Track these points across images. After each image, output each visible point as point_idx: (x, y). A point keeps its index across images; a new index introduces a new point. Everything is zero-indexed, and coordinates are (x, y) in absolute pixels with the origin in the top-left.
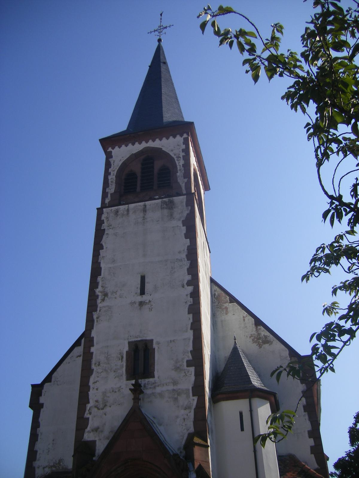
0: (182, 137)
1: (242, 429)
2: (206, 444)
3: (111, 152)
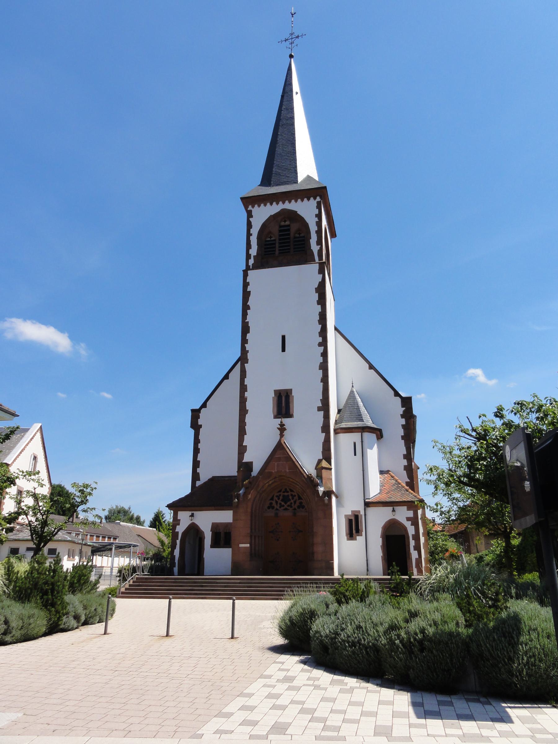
0: (315, 200)
1: (355, 455)
2: (330, 467)
3: (251, 211)
